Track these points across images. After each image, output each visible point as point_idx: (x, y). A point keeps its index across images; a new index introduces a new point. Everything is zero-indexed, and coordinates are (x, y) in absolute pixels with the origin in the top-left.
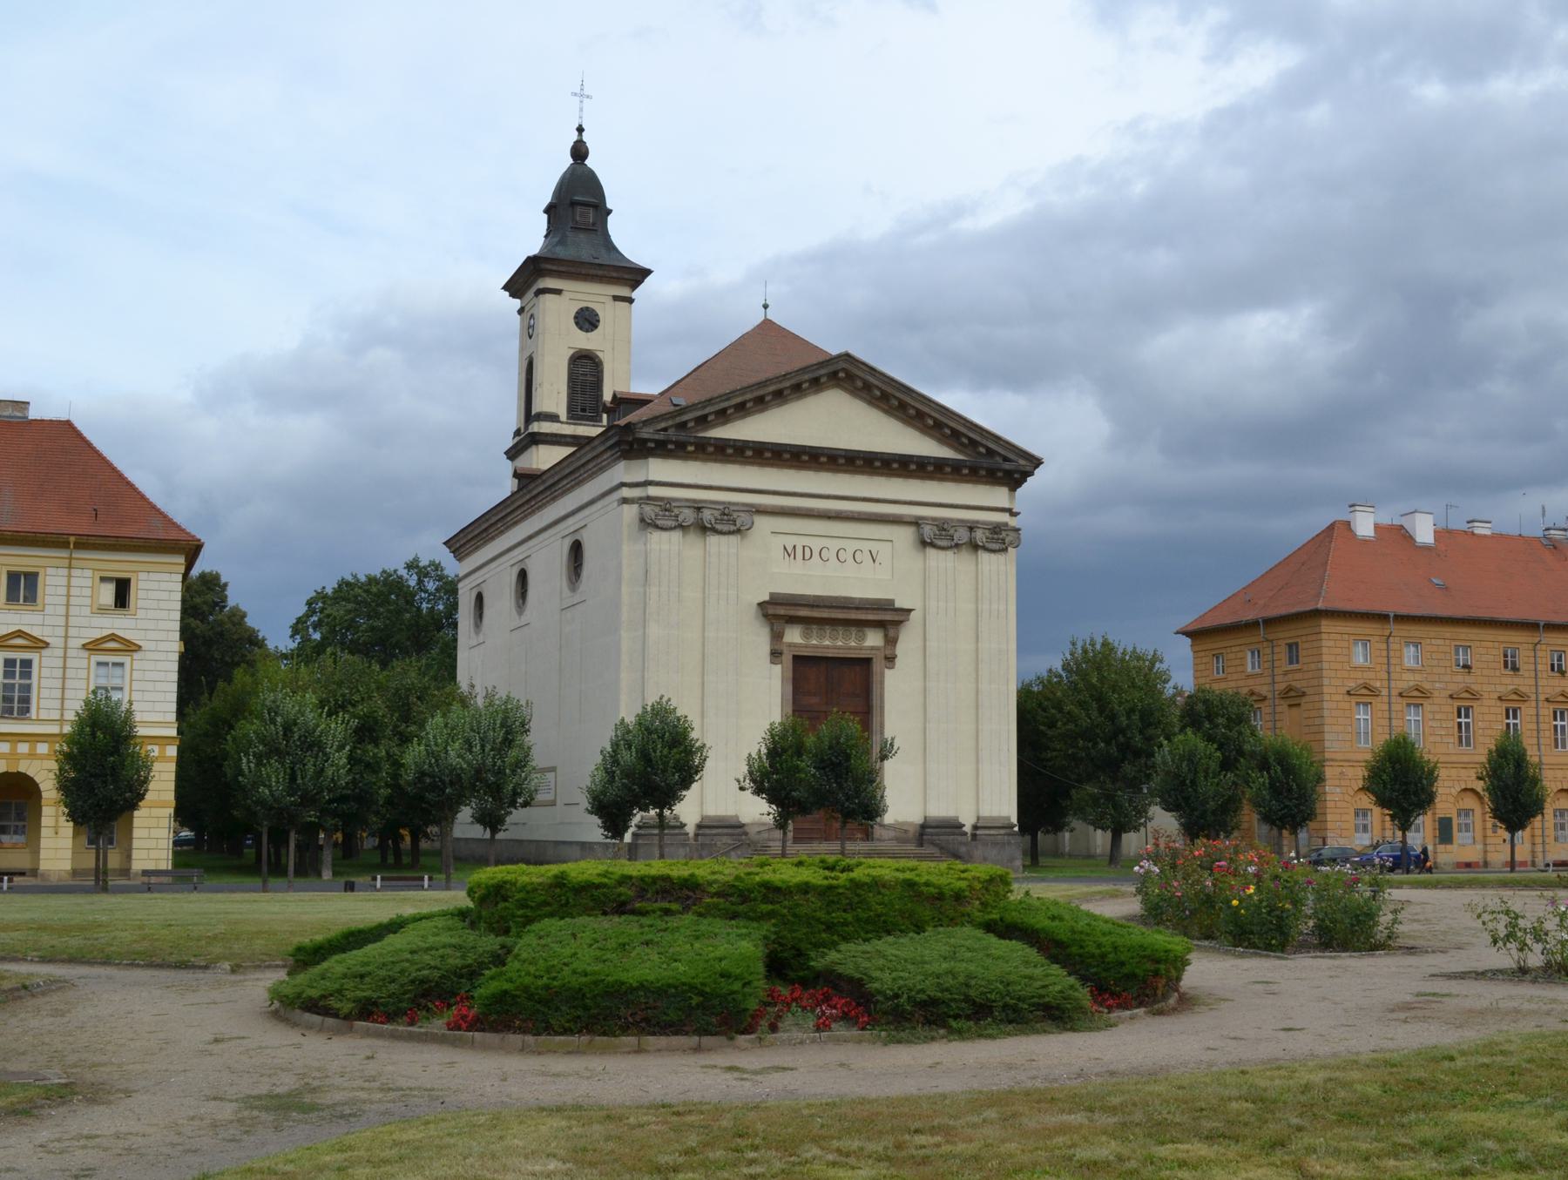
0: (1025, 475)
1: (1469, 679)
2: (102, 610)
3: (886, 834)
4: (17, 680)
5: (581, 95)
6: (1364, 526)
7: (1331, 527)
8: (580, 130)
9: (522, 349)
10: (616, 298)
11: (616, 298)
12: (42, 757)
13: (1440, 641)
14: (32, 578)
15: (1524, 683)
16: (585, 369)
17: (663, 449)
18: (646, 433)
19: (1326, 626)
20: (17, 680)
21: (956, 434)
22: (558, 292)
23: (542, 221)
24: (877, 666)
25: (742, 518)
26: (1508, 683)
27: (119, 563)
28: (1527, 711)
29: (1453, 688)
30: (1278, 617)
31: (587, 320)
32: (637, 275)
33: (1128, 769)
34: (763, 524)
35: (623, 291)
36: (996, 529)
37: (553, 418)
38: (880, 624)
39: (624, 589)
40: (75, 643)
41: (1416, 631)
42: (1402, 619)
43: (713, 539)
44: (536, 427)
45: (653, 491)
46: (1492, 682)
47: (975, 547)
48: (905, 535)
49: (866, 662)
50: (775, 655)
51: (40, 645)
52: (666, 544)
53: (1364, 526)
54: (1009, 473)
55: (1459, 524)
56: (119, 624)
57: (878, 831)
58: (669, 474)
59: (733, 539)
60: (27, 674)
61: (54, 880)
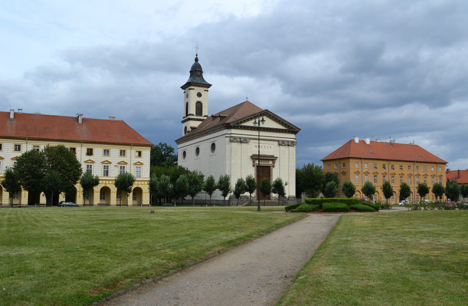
0: (298, 132)
1: (376, 170)
2: (136, 157)
3: (273, 198)
4: (122, 170)
5: (197, 48)
6: (357, 140)
7: (351, 141)
8: (197, 55)
9: (185, 100)
10: (205, 90)
11: (205, 90)
12: (111, 184)
13: (371, 163)
14: (124, 151)
15: (386, 171)
16: (199, 106)
17: (234, 127)
18: (232, 124)
19: (351, 160)
20: (122, 170)
21: (286, 124)
22: (194, 89)
23: (189, 74)
24: (271, 168)
25: (248, 140)
26: (384, 171)
27: (139, 149)
28: (387, 176)
29: (374, 172)
30: (341, 159)
31: (199, 95)
32: (209, 86)
33: (316, 187)
34: (251, 141)
35: (206, 89)
36: (293, 142)
37: (193, 115)
38: (272, 160)
39: (227, 153)
40: (132, 163)
41: (367, 161)
42: (364, 159)
43: (243, 144)
44: (189, 117)
45: (232, 135)
46: (381, 170)
47: (288, 145)
48: (277, 143)
49: (269, 167)
50: (254, 165)
51: (126, 163)
52: (234, 145)
53: (357, 140)
54: (295, 132)
55: (374, 140)
56: (139, 160)
57: (271, 198)
58: (235, 132)
59: (246, 144)
60: (108, 168)
61: (24, 206)
